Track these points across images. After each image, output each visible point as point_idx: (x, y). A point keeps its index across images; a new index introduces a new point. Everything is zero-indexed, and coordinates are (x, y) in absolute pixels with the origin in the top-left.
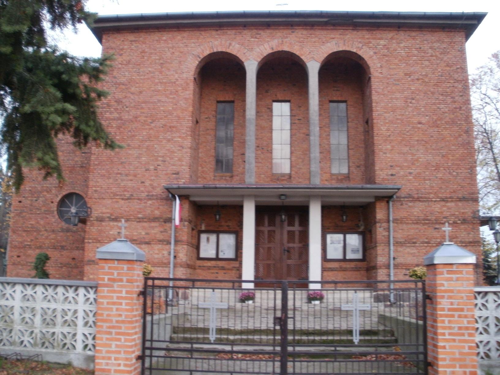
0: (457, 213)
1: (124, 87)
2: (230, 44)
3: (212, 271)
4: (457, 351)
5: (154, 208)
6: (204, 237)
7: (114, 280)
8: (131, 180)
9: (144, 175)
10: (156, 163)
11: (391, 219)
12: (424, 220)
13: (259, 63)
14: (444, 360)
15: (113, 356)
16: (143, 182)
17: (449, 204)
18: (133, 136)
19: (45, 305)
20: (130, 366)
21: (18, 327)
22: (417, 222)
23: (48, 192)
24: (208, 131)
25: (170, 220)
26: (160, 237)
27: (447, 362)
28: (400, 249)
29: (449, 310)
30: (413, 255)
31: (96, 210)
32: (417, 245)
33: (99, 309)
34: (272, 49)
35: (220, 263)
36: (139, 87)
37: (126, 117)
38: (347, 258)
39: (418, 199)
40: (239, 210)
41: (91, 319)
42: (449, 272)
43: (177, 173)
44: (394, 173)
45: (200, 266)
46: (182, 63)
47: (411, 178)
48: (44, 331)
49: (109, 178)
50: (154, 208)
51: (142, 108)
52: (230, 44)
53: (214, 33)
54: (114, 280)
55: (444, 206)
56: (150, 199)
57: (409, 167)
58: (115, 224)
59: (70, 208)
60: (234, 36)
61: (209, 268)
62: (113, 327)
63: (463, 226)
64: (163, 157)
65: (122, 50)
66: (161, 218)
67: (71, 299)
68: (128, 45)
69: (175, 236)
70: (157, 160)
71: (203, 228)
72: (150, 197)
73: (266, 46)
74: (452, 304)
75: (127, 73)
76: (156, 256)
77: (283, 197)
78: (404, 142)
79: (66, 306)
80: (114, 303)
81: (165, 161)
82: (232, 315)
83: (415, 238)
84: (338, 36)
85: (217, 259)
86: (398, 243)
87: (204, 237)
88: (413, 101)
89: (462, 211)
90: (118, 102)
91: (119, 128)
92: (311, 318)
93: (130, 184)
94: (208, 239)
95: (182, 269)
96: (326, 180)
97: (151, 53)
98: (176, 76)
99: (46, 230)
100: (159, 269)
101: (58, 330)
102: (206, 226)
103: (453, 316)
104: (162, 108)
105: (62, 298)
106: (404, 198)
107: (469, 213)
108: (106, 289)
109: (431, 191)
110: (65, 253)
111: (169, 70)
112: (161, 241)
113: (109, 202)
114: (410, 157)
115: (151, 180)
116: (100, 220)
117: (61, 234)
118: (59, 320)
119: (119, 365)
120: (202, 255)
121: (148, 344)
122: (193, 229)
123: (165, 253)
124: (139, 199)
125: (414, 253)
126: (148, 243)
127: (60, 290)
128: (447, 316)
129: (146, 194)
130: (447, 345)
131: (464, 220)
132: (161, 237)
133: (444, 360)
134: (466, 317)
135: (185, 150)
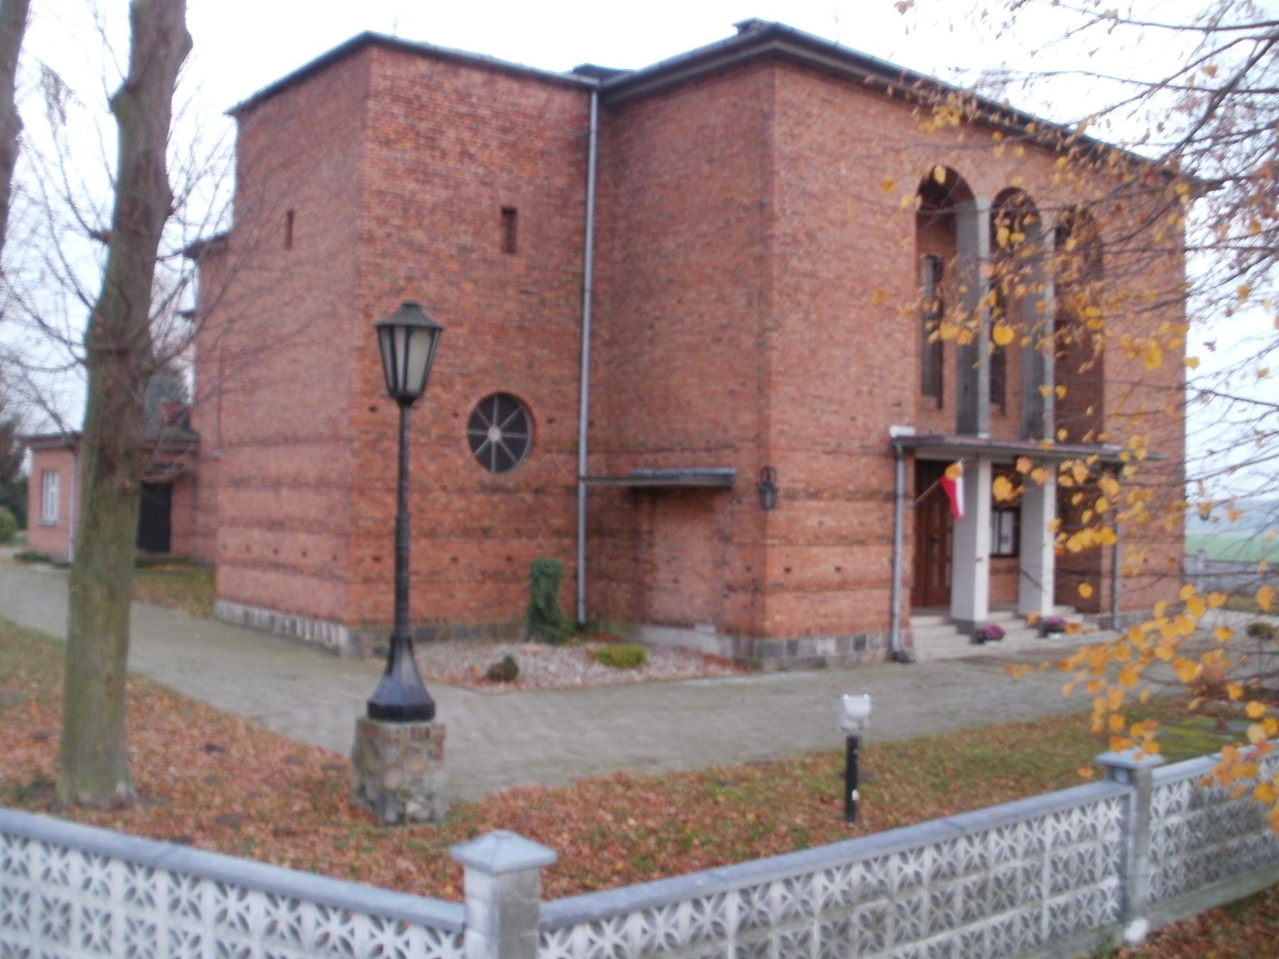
8: (836, 413)
23: (444, 386)
51: (847, 260)
59: (486, 429)
72: (865, 451)
91: (814, 295)
99: (444, 488)
110: (489, 544)
116: (792, 495)
117: (480, 498)
126: (862, 543)
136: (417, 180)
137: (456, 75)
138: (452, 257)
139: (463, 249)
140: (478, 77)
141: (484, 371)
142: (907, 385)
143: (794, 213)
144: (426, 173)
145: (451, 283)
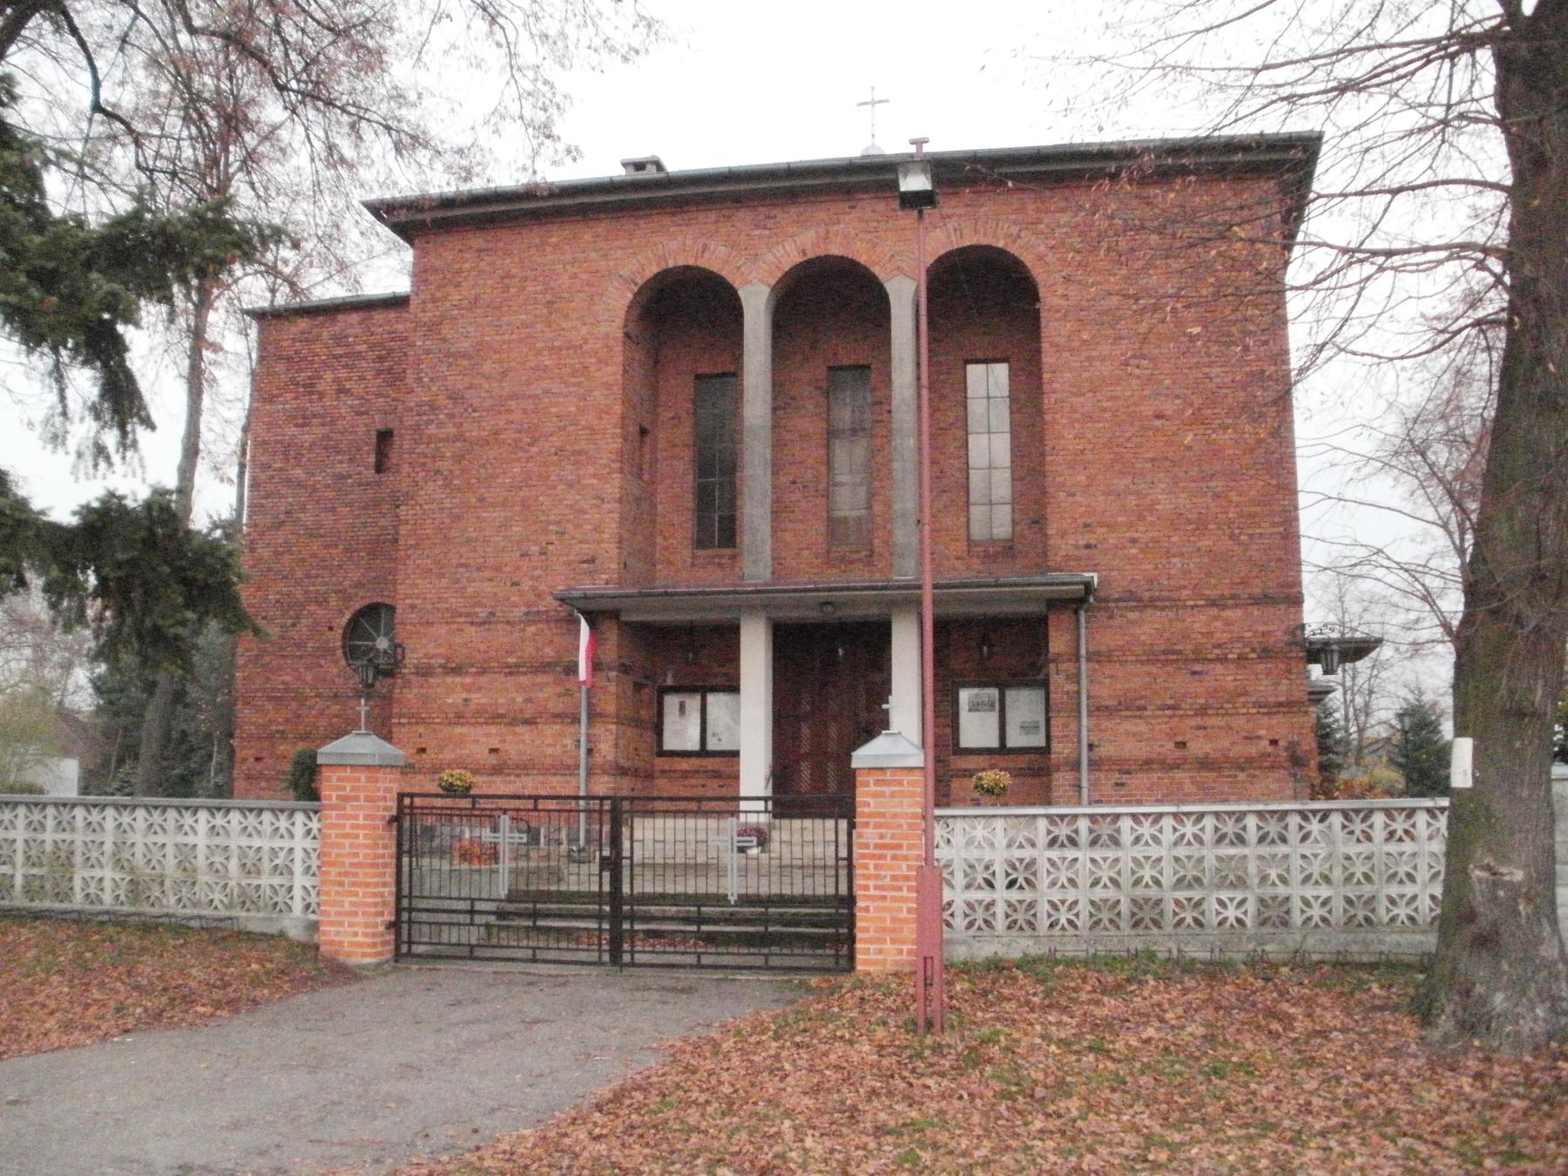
0: (1247, 634)
1: (465, 363)
2: (705, 248)
3: (694, 781)
4: (887, 915)
5: (537, 642)
6: (671, 702)
7: (346, 799)
9: (518, 568)
10: (543, 539)
11: (1083, 652)
12: (1166, 652)
13: (773, 289)
14: (866, 930)
15: (346, 920)
16: (515, 584)
17: (1228, 613)
18: (492, 476)
19: (244, 842)
20: (374, 935)
21: (203, 878)
22: (1151, 658)
23: (320, 604)
24: (676, 450)
25: (572, 669)
26: (557, 706)
27: (872, 934)
28: (1105, 724)
29: (877, 846)
30: (1138, 736)
31: (414, 651)
32: (1148, 713)
33: (324, 845)
34: (804, 253)
35: (710, 763)
36: (500, 362)
37: (473, 432)
38: (1011, 743)
39: (1152, 603)
40: (726, 639)
41: (315, 863)
42: (877, 782)
43: (592, 561)
44: (1093, 542)
45: (663, 772)
46: (596, 298)
47: (1133, 551)
48: (243, 883)
49: (441, 576)
50: (537, 642)
51: (510, 411)
52: (705, 248)
53: (667, 220)
54: (346, 799)
55: (1216, 618)
56: (534, 622)
57: (1131, 525)
58: (458, 679)
60: (713, 227)
61: (686, 774)
62: (346, 874)
63: (1262, 666)
64: (558, 523)
65: (459, 272)
66: (557, 664)
67: (283, 831)
68: (478, 261)
69: (590, 705)
70: (546, 531)
71: (670, 682)
72: (532, 617)
73: (790, 246)
74: (881, 836)
75: (471, 329)
76: (549, 751)
77: (829, 609)
78: (1117, 467)
79: (277, 843)
80: (346, 836)
81: (563, 534)
82: (670, 874)
83: (1142, 697)
84: (962, 211)
85: (703, 752)
86: (1098, 710)
87: (671, 702)
88: (1145, 363)
89: (1261, 628)
90: (456, 398)
91: (458, 459)
92: (798, 874)
93: (488, 588)
94: (682, 707)
95: (606, 778)
96: (958, 558)
97: (525, 279)
98: (584, 331)
99: (318, 695)
100: (555, 779)
101: (265, 881)
102: (674, 676)
103: (881, 857)
104: (554, 410)
105: (269, 829)
106: (1117, 600)
107: (1279, 634)
108: (334, 813)
109: (1182, 583)
111: (566, 317)
112: (558, 717)
113: (443, 630)
114: (1132, 501)
115: (532, 578)
116: (425, 672)
118: (266, 866)
119: (356, 934)
120: (670, 744)
121: (405, 903)
122: (638, 687)
123: (569, 742)
124: (508, 622)
125: (1141, 734)
127: (267, 817)
128: (873, 856)
129: (523, 609)
130: (872, 905)
131: (1264, 650)
132: (560, 708)
133: (866, 930)
134: (905, 858)
135: (606, 506)
136: (296, 425)
137: (334, 320)
138: (328, 486)
139: (341, 477)
140: (354, 318)
141: (359, 585)
142: (605, 536)
143: (432, 380)
144: (304, 417)
145: (326, 510)
